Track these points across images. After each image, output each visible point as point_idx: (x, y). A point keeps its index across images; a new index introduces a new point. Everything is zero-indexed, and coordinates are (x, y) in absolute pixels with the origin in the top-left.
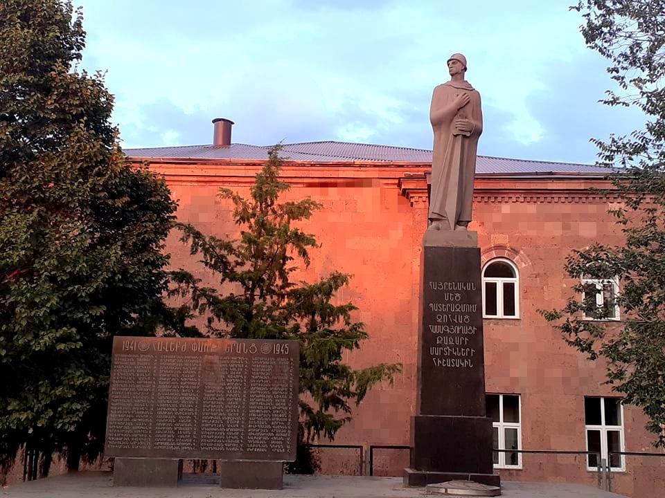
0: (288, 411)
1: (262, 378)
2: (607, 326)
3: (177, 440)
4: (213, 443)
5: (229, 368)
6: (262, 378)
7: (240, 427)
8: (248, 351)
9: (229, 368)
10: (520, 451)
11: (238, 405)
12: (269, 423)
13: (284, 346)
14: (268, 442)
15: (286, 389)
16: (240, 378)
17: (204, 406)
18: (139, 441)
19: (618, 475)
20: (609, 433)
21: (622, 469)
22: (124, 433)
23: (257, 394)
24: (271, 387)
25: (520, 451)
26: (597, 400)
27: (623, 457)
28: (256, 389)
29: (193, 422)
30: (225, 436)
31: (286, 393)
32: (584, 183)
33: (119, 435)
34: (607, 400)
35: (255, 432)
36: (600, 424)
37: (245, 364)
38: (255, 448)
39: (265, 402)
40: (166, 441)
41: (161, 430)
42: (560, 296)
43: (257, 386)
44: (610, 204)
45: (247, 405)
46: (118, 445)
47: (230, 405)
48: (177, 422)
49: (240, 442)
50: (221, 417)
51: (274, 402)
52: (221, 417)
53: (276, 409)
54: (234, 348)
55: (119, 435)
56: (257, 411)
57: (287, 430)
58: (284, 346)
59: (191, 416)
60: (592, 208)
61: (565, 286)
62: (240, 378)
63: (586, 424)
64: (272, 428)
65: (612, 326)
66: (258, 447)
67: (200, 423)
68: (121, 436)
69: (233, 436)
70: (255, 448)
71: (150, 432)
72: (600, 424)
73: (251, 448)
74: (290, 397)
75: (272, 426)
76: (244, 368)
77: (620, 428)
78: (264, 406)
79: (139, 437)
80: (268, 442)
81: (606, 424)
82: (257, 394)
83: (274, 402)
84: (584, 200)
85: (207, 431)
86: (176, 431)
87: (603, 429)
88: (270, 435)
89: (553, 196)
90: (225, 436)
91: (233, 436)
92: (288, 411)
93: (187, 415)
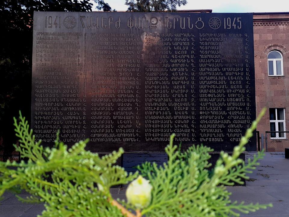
0: (245, 94)
1: (212, 56)
2: (278, 78)
3: (117, 131)
4: (160, 132)
5: (172, 46)
6: (212, 56)
7: (189, 114)
8: (194, 26)
9: (172, 46)
10: (285, 132)
11: (185, 89)
12: (224, 108)
13: (236, 20)
14: (225, 130)
15: (242, 69)
16: (186, 58)
17: (146, 91)
18: (72, 134)
19: (284, 141)
20: (279, 123)
21: (285, 138)
22: (52, 124)
23: (208, 75)
24: (224, 67)
25: (285, 132)
26: (274, 109)
27: (285, 133)
28: (206, 70)
29: (134, 110)
30: (172, 124)
31: (242, 74)
32: (270, 16)
33: (47, 127)
34: (278, 109)
35: (208, 119)
36: (275, 119)
37: (191, 41)
38: (209, 137)
39: (218, 85)
40: (104, 133)
41: (98, 120)
42: (259, 66)
43: (208, 66)
44: (279, 26)
45: (197, 90)
46: (46, 138)
47: (177, 90)
48: (116, 110)
49: (191, 132)
50: (167, 103)
51: (229, 85)
52: (167, 103)
53: (232, 93)
54: (177, 24)
55: (47, 127)
56: (209, 95)
57: (246, 115)
58: (236, 20)
59: (131, 103)
60: (272, 28)
61: (261, 62)
62: (186, 58)
63: (270, 120)
64: (228, 115)
65: (280, 78)
66: (213, 137)
67: (197, 98)
68: (49, 128)
69: (183, 124)
70: (209, 137)
71: (84, 122)
72: (275, 119)
73: (205, 138)
74: (247, 78)
75: (227, 112)
76: (190, 46)
77: (284, 121)
78: (216, 89)
79: (71, 129)
80: (225, 130)
81: (278, 120)
82: (208, 75)
83: (229, 85)
84: (268, 24)
85: (152, 120)
86: (115, 121)
87: (277, 122)
88: (225, 122)
89: (255, 22)
90: (172, 124)
91: (183, 124)
92: (245, 94)
93: (127, 102)
